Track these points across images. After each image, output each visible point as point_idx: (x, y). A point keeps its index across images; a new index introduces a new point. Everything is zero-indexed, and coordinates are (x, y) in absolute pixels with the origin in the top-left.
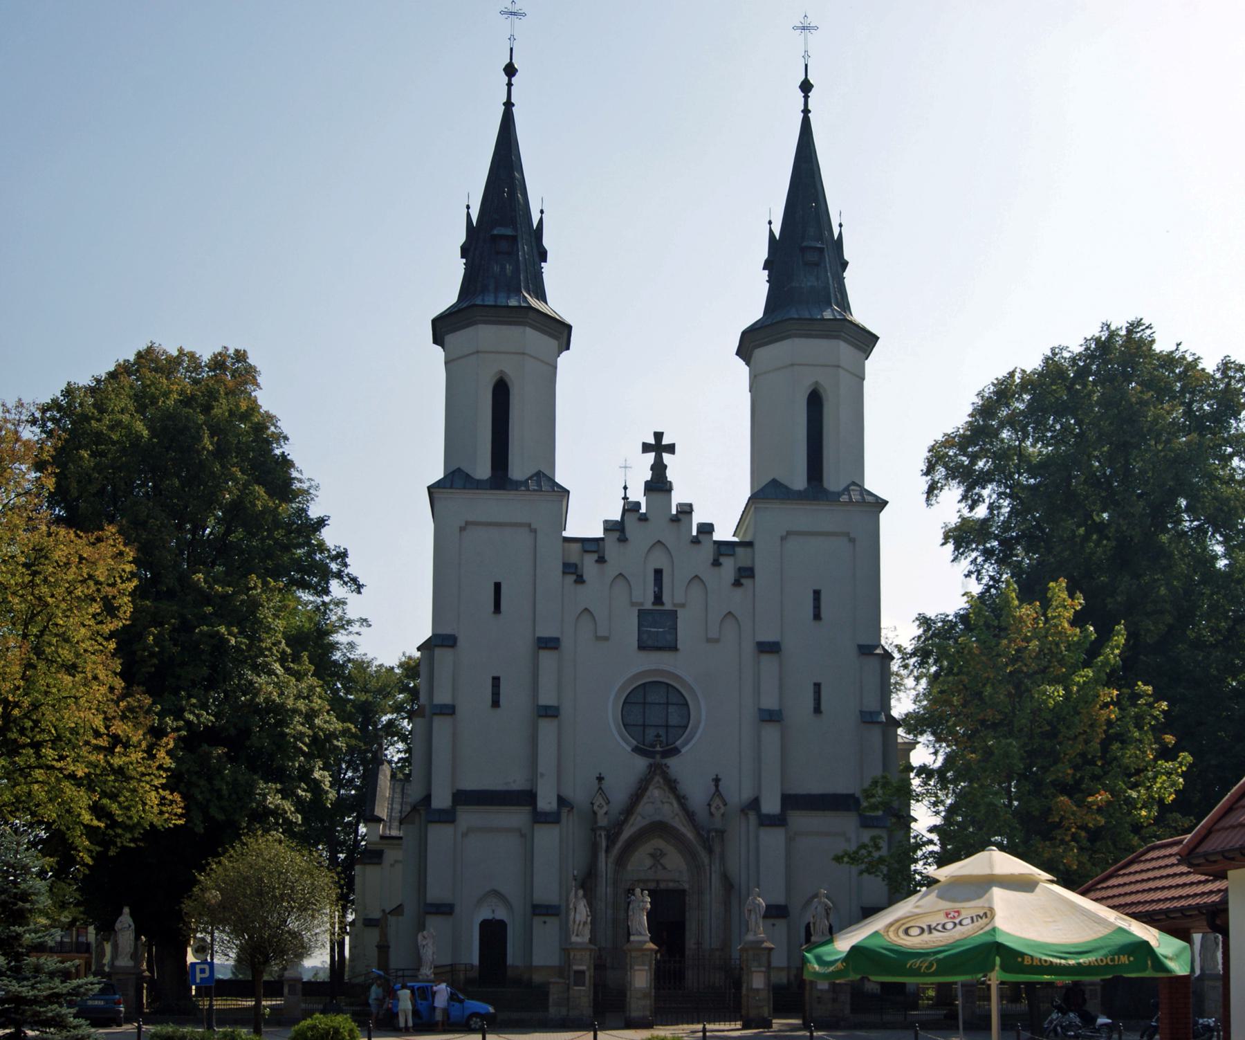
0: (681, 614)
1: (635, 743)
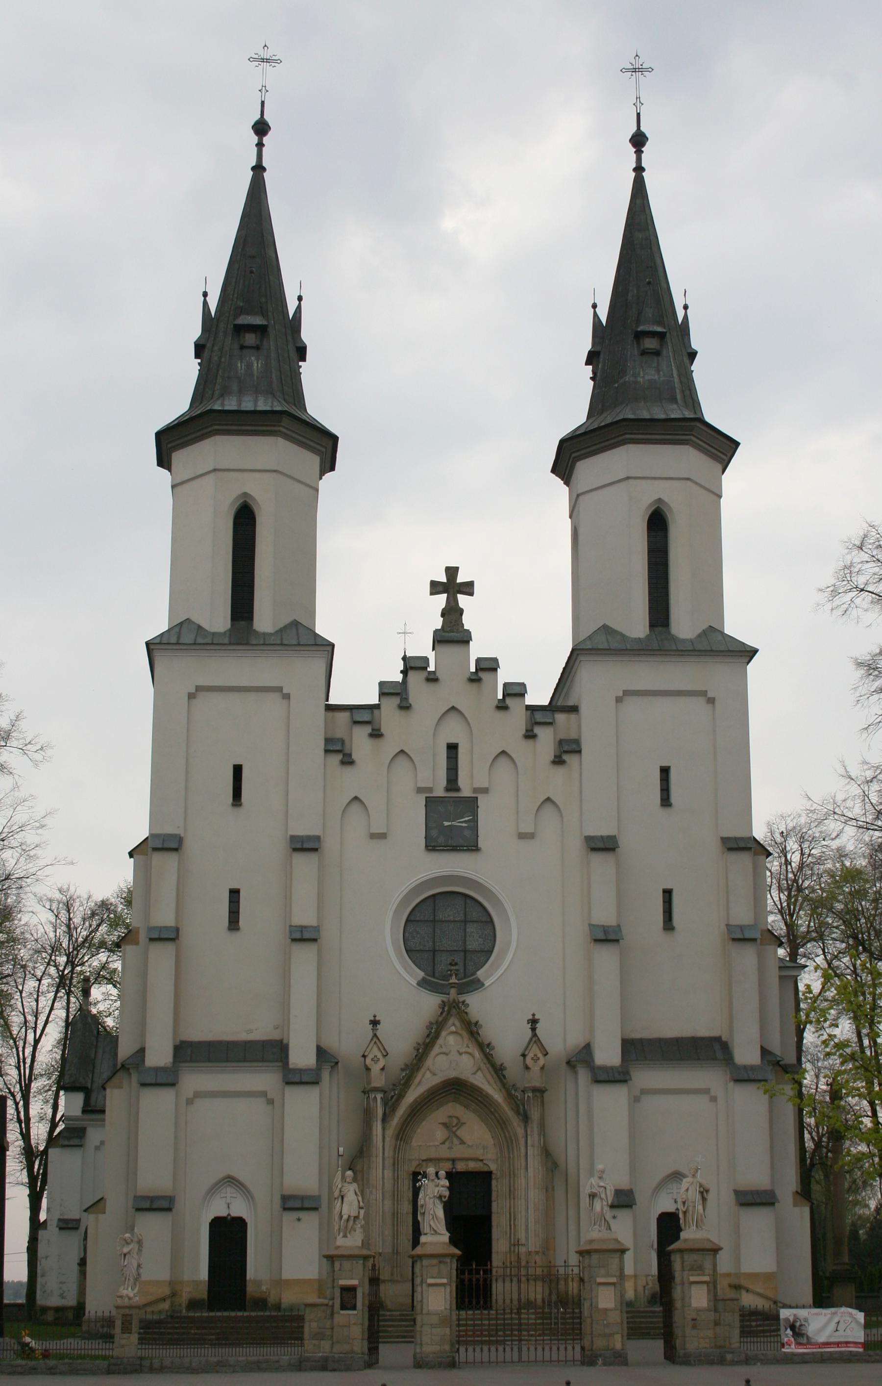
0: (482, 801)
1: (421, 974)
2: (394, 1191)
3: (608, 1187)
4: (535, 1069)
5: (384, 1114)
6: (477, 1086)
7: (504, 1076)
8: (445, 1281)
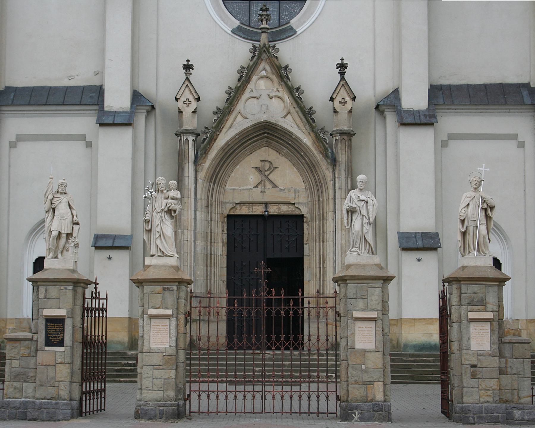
1: (237, 23)
2: (207, 233)
3: (370, 201)
4: (343, 112)
5: (196, 157)
6: (286, 130)
7: (313, 120)
8: (169, 312)
